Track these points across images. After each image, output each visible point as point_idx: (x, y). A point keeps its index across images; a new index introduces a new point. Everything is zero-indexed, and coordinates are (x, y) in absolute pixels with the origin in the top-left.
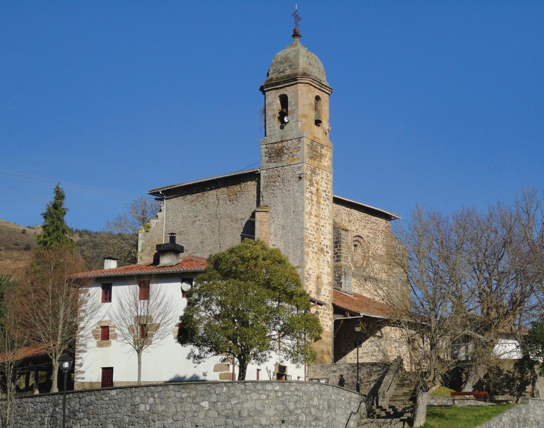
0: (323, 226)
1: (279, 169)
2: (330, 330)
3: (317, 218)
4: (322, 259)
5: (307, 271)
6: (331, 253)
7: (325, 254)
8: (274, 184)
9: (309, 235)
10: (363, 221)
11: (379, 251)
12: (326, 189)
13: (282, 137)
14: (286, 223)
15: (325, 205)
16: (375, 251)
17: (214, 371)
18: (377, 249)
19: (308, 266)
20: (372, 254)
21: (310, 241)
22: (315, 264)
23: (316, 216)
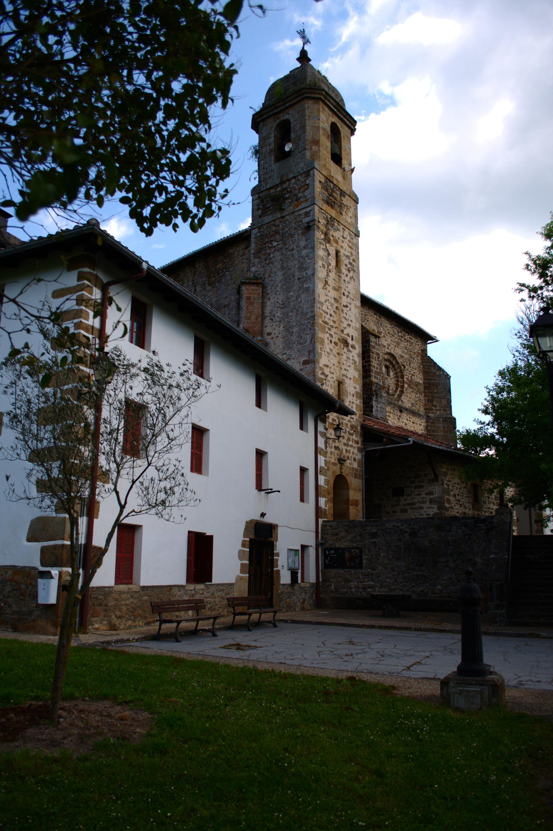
0: (347, 306)
1: (277, 222)
2: (358, 466)
3: (336, 292)
4: (345, 355)
5: (321, 369)
6: (358, 349)
7: (350, 348)
8: (270, 245)
9: (324, 314)
10: (396, 336)
11: (415, 377)
12: (349, 254)
13: (282, 177)
14: (288, 298)
15: (349, 277)
16: (411, 377)
17: (29, 540)
18: (414, 375)
19: (323, 361)
20: (407, 379)
21: (326, 323)
22: (334, 360)
23: (335, 289)
